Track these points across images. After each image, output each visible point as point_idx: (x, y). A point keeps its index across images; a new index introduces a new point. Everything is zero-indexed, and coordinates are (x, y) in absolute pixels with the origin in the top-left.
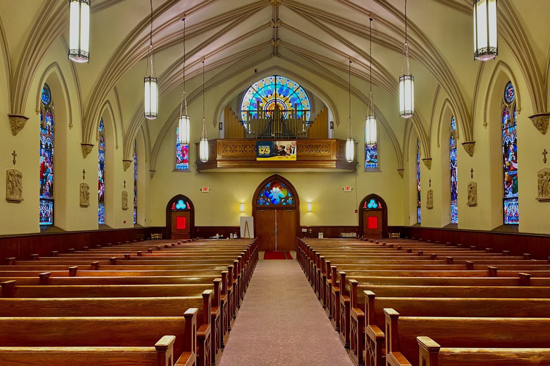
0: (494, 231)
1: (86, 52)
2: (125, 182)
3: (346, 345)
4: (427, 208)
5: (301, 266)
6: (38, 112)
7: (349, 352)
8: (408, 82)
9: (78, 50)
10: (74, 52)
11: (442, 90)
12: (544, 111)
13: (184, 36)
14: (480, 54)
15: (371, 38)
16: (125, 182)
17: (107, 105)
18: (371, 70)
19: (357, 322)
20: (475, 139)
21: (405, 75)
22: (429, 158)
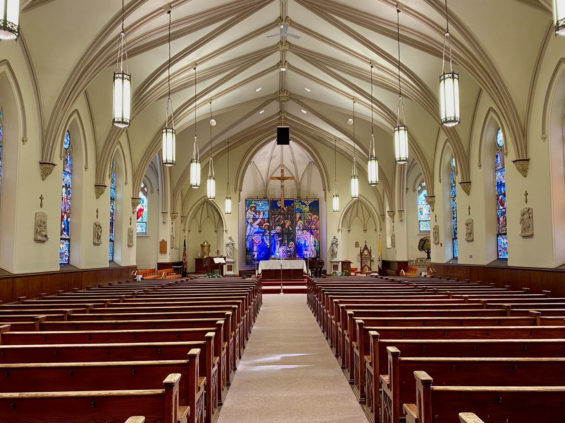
0: (448, 263)
1: (15, 25)
2: (97, 211)
3: (342, 366)
4: (466, 241)
5: (309, 306)
6: (24, 141)
7: (353, 388)
8: (449, 81)
9: (121, 119)
10: (118, 120)
11: (484, 94)
12: (525, 157)
13: (169, 33)
14: (562, 26)
15: (399, 26)
16: (97, 211)
17: (75, 115)
18: (373, 109)
19: (372, 376)
20: (530, 155)
21: (445, 73)
22: (525, 158)
